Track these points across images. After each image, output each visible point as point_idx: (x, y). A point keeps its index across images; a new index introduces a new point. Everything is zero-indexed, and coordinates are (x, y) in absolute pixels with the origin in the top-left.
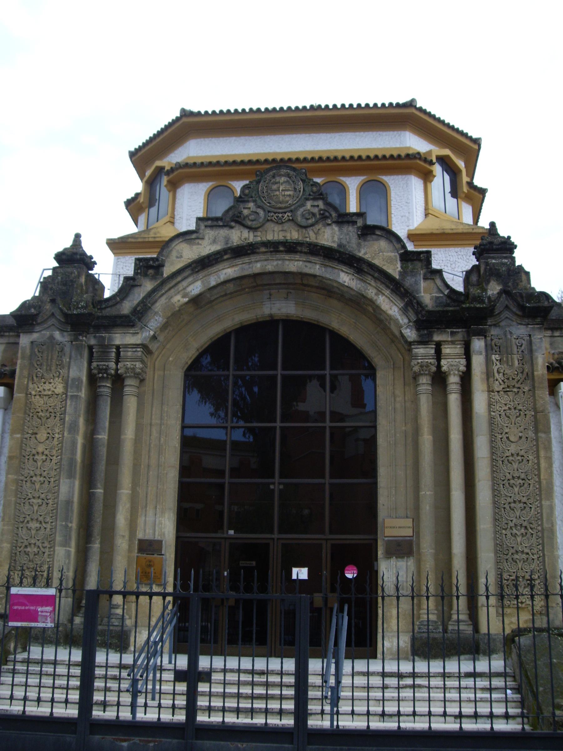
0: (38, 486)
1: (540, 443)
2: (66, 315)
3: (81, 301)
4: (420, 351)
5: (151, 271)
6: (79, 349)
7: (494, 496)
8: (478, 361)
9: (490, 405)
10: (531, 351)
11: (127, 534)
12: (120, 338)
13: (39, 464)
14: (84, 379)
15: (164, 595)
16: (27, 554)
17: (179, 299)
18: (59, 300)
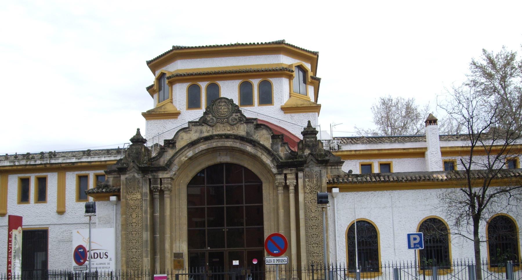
0: (134, 235)
2: (139, 167)
3: (144, 161)
4: (278, 177)
5: (171, 145)
6: (145, 180)
7: (306, 232)
8: (300, 181)
9: (305, 198)
10: (321, 177)
11: (170, 251)
12: (161, 175)
13: (134, 227)
14: (148, 192)
15: (186, 274)
16: (133, 261)
17: (184, 159)
18: (136, 161)
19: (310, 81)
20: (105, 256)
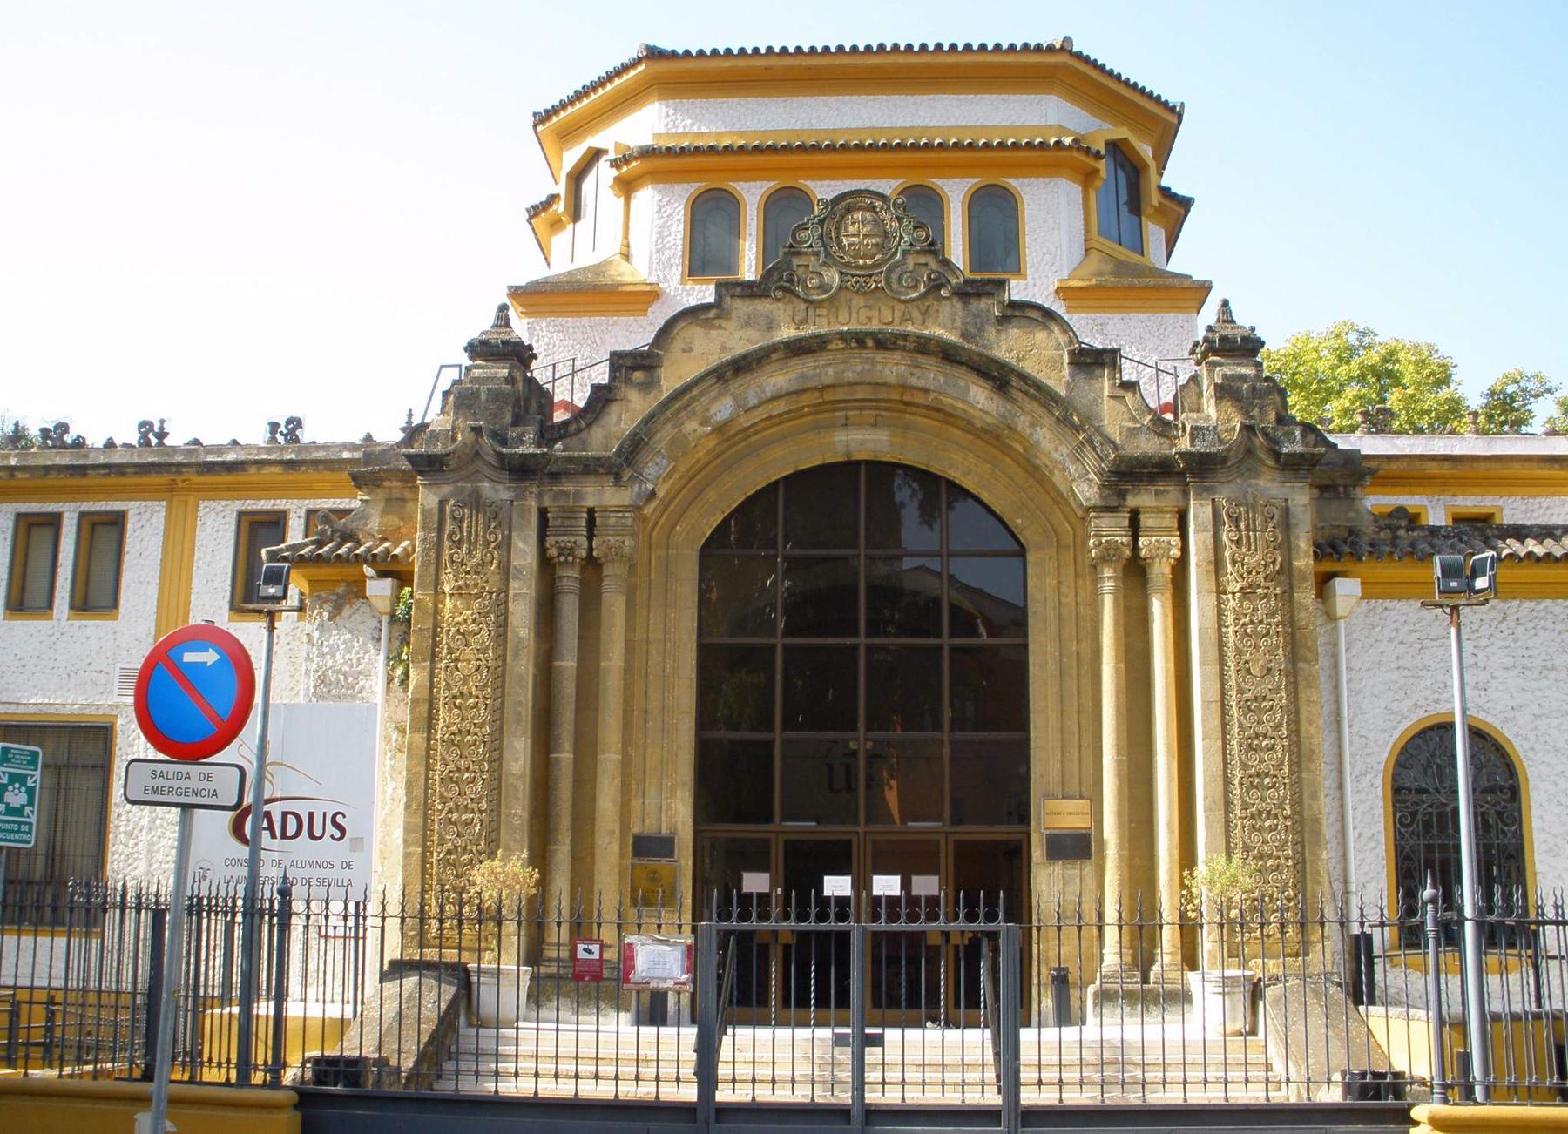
1: (1300, 679)
19: (1155, 203)
20: (331, 830)
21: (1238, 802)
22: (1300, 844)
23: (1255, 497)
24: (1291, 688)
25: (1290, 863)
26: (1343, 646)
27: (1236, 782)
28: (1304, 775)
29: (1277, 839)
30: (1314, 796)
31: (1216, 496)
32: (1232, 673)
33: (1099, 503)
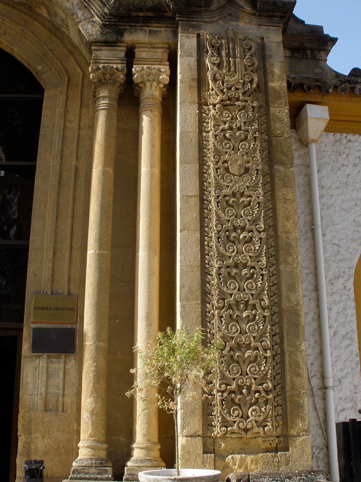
1: (277, 180)
21: (215, 292)
22: (278, 336)
23: (235, 34)
24: (268, 187)
25: (269, 354)
26: (315, 168)
27: (214, 272)
28: (282, 267)
29: (254, 330)
30: (292, 288)
31: (201, 32)
32: (212, 172)
33: (100, 38)
